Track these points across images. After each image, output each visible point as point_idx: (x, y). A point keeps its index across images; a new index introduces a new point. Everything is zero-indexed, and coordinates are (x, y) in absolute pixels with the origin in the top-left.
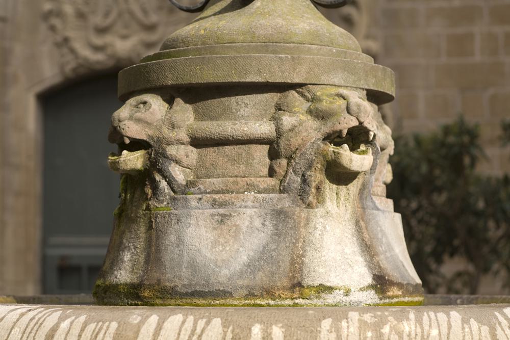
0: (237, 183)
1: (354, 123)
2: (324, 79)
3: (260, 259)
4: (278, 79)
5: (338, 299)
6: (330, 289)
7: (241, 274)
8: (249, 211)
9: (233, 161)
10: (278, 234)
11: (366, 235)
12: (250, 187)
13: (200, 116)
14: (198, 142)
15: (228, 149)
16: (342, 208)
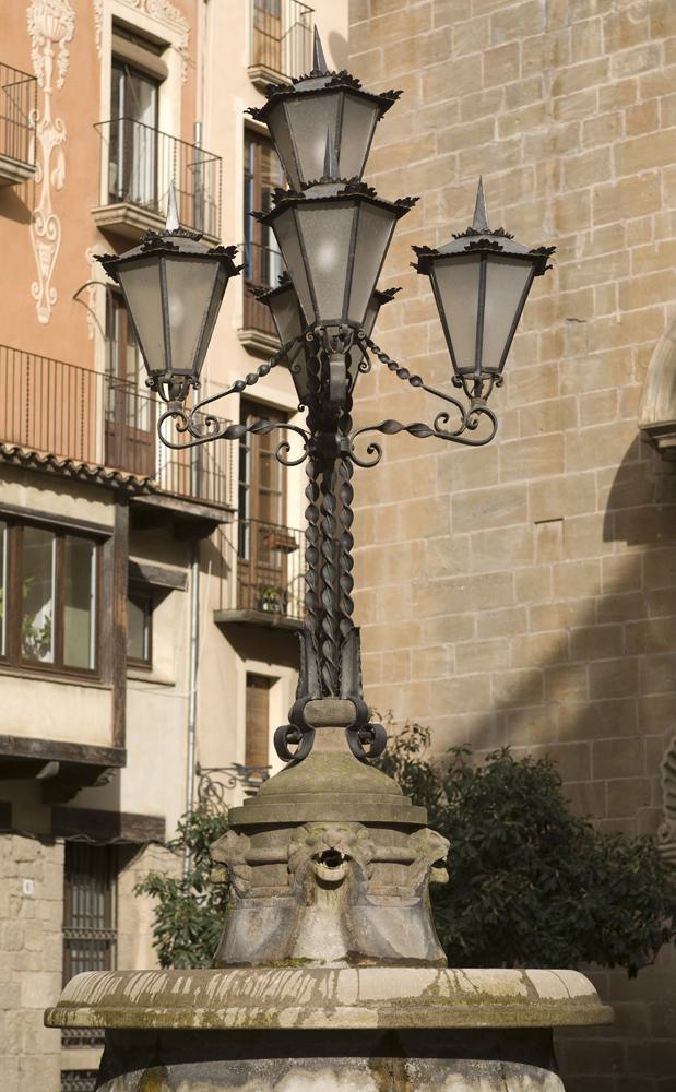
0: (267, 890)
1: (327, 848)
2: (318, 818)
3: (270, 941)
4: (287, 820)
5: (316, 966)
6: (310, 960)
7: (258, 951)
8: (268, 909)
9: (268, 875)
10: (283, 924)
11: (350, 924)
12: (275, 893)
13: (255, 845)
14: (252, 863)
15: (266, 866)
16: (331, 906)
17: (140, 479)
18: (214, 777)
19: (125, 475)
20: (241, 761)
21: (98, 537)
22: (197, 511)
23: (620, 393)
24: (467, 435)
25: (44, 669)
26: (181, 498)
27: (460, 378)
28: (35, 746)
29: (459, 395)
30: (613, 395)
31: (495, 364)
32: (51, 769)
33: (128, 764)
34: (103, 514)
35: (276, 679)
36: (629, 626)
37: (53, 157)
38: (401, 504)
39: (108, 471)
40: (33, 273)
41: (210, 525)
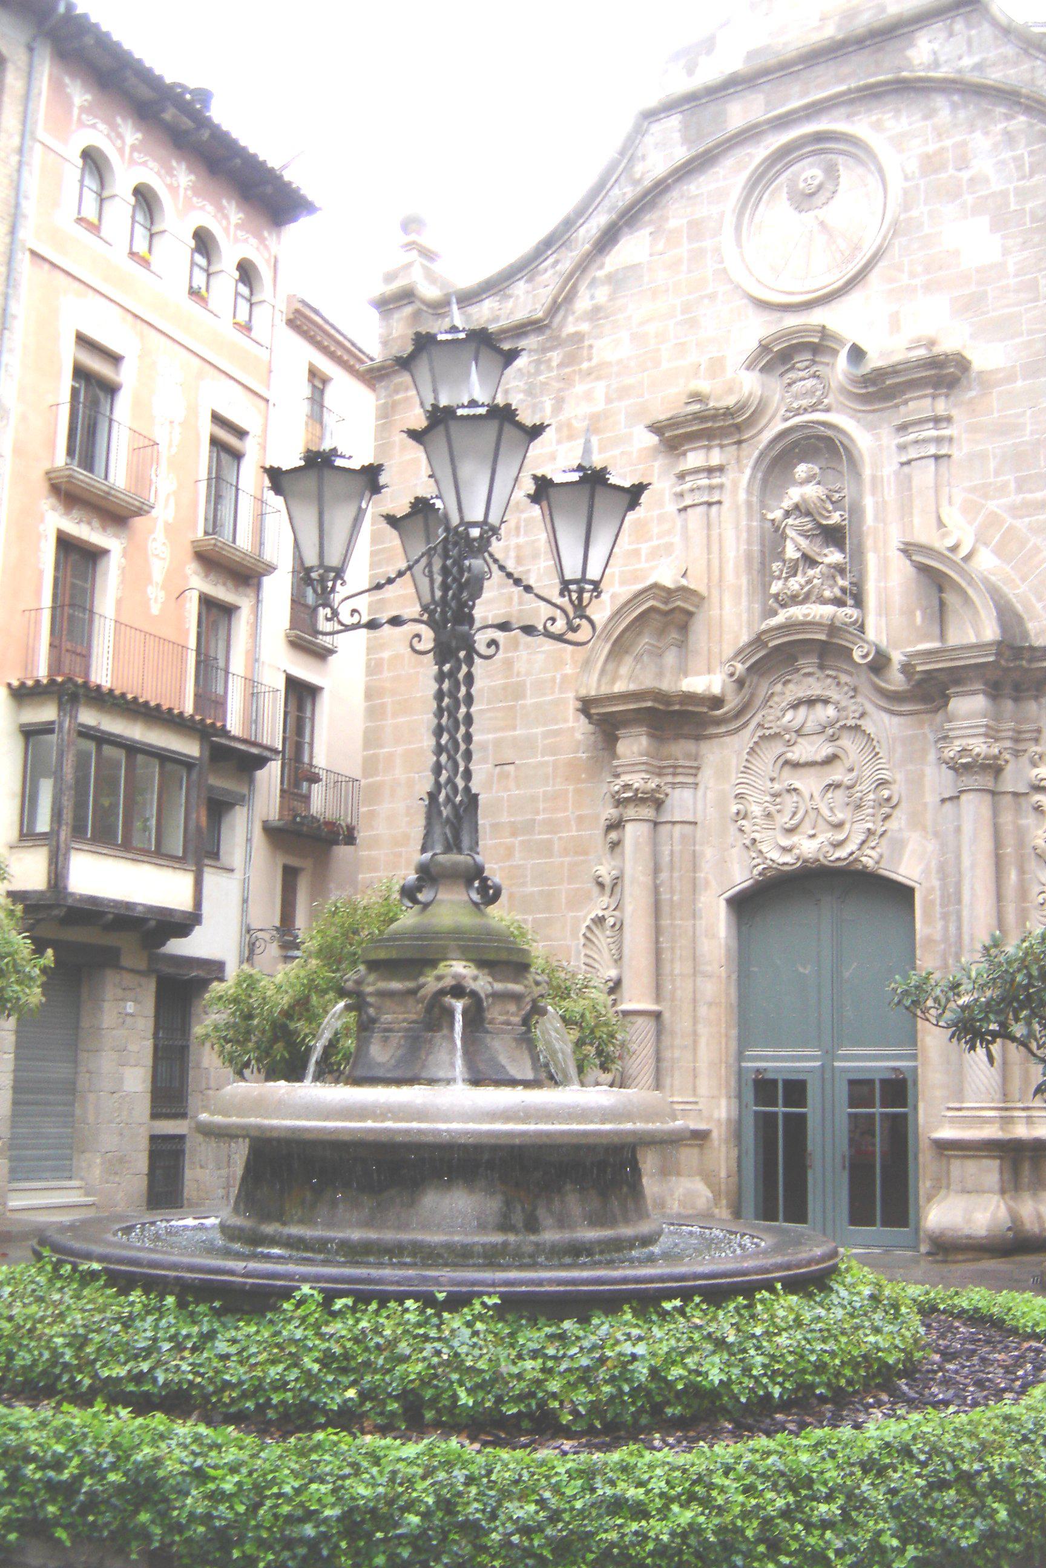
17: (219, 724)
18: (260, 934)
19: (209, 721)
20: (278, 924)
21: (186, 763)
22: (255, 751)
23: (558, 676)
24: (570, 636)
25: (145, 852)
26: (245, 741)
27: (565, 586)
28: (140, 908)
29: (564, 601)
30: (554, 679)
31: (597, 578)
32: (153, 923)
33: (204, 921)
34: (190, 748)
35: (302, 869)
36: (560, 838)
37: (167, 500)
38: (400, 749)
39: (198, 718)
40: (149, 580)
41: (260, 762)
